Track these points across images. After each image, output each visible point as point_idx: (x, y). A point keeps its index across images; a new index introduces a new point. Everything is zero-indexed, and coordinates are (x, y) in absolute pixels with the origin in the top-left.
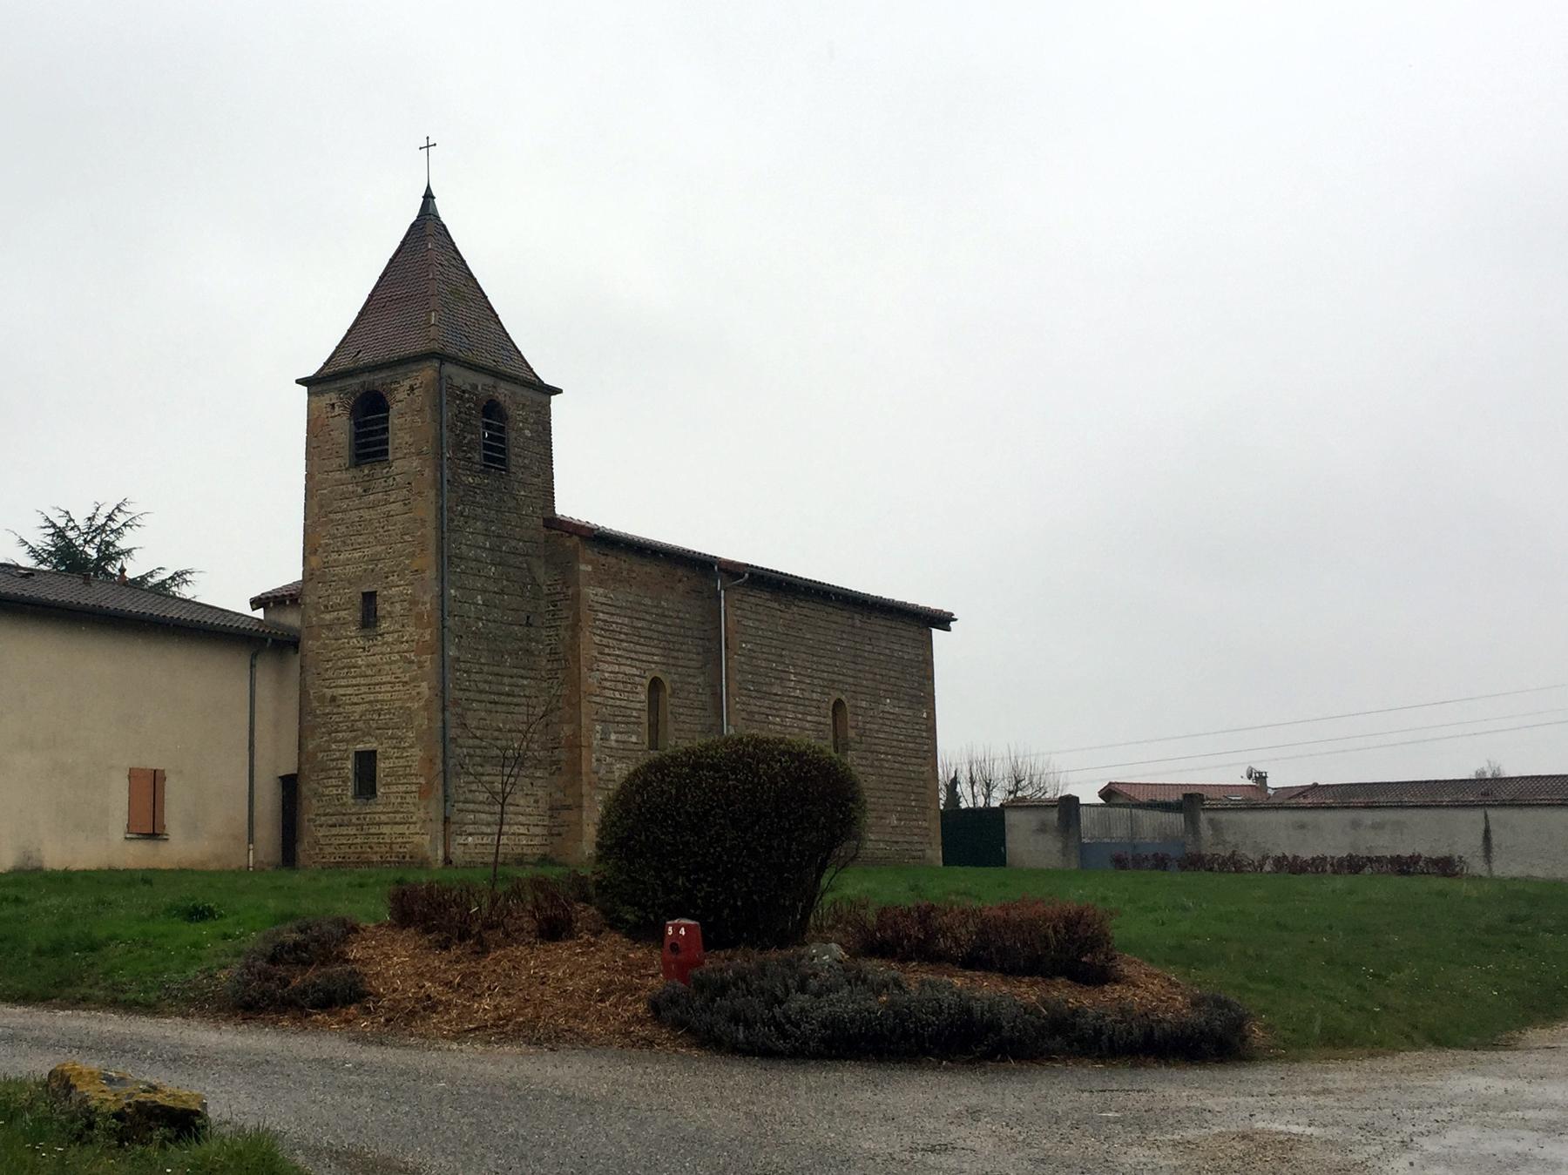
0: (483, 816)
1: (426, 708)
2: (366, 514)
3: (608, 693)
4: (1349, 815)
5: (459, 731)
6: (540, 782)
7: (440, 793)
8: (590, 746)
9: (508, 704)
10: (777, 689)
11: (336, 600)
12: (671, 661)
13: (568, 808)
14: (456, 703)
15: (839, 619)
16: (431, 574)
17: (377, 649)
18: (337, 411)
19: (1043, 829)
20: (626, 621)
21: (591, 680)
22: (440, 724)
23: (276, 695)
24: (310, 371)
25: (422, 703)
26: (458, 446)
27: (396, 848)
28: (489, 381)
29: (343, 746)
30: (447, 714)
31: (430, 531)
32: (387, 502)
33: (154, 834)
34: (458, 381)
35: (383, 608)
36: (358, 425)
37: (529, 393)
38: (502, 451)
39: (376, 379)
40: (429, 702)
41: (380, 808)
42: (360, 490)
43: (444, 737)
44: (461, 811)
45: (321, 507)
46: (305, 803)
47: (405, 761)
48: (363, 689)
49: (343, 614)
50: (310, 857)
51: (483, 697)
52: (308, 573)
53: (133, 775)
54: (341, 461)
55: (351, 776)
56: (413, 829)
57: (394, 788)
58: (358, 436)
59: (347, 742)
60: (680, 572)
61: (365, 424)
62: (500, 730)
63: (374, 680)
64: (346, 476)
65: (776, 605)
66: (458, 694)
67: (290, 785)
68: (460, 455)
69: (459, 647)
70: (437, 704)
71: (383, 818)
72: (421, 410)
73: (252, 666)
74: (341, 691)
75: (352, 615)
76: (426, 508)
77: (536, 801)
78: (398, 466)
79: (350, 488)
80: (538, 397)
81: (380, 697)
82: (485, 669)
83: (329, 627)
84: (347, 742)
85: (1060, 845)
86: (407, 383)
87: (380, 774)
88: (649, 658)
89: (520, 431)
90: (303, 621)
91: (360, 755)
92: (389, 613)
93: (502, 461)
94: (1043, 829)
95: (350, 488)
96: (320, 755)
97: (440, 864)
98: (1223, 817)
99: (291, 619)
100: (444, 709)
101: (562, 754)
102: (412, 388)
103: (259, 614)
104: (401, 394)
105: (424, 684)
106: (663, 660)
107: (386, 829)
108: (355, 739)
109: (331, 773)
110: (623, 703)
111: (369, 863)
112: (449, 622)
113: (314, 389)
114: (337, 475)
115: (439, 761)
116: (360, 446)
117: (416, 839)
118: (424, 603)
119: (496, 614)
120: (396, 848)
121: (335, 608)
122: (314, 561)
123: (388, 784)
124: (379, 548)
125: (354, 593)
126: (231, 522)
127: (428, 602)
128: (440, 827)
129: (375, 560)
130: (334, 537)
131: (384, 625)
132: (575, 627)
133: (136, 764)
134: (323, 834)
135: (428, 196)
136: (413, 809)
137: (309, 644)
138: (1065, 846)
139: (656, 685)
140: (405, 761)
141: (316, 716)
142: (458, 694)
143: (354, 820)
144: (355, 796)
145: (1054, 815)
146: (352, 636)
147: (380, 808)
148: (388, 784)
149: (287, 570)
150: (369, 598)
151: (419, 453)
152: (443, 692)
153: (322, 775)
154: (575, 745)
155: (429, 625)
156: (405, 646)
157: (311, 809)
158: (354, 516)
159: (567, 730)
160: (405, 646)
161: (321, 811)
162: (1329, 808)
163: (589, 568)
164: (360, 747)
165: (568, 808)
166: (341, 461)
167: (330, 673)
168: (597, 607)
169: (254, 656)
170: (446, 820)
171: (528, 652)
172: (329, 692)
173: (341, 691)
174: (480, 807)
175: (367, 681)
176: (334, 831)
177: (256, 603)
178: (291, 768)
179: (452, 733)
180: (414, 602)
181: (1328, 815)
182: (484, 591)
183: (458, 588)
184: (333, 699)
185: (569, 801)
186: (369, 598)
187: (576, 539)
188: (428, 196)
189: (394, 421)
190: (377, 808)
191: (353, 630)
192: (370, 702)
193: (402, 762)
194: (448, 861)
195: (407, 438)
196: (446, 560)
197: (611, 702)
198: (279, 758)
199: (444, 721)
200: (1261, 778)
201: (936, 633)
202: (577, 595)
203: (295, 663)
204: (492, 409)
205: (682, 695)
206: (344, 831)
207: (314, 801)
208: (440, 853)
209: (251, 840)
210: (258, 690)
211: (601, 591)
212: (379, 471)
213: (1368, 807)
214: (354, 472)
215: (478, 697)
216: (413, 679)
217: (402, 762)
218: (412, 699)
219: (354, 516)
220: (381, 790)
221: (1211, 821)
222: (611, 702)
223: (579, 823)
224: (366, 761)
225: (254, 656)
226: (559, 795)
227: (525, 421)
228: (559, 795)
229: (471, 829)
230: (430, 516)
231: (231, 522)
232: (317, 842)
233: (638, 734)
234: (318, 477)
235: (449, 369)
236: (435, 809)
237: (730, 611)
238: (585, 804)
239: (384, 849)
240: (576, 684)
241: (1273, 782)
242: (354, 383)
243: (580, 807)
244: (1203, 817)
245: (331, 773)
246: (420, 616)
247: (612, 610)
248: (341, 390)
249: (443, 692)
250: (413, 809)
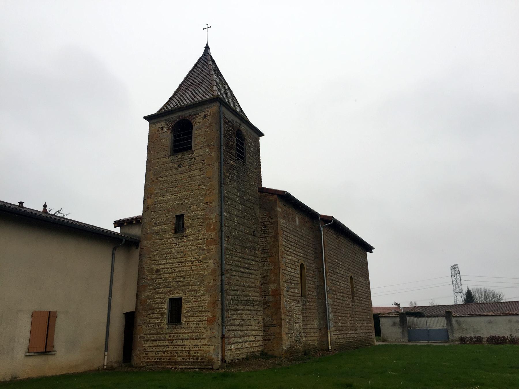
1: (212, 274)
2: (179, 177)
3: (288, 269)
4: (508, 318)
6: (259, 313)
7: (220, 322)
8: (283, 295)
9: (247, 273)
11: (161, 219)
12: (306, 256)
13: (274, 326)
14: (227, 270)
16: (215, 204)
17: (183, 244)
18: (165, 130)
19: (394, 324)
20: (292, 237)
21: (283, 262)
22: (220, 283)
23: (126, 268)
24: (154, 111)
25: (209, 271)
26: (227, 145)
27: (193, 353)
28: (239, 121)
29: (162, 296)
30: (224, 276)
31: (215, 182)
32: (191, 170)
33: (47, 350)
34: (227, 116)
35: (187, 222)
36: (175, 137)
39: (186, 114)
40: (214, 270)
41: (183, 330)
42: (176, 166)
43: (222, 290)
44: (229, 330)
45: (155, 175)
46: (139, 327)
47: (198, 304)
48: (175, 265)
49: (164, 226)
50: (140, 358)
51: (238, 269)
52: (146, 209)
53: (35, 315)
54: (166, 153)
55: (166, 312)
56: (205, 342)
57: (192, 319)
58: (175, 141)
59: (165, 293)
62: (244, 286)
63: (181, 260)
64: (168, 159)
67: (130, 319)
68: (228, 149)
69: (228, 242)
70: (218, 272)
71: (185, 336)
72: (210, 126)
73: (113, 254)
74: (162, 266)
75: (170, 227)
76: (213, 171)
77: (258, 323)
78: (196, 153)
79: (171, 165)
80: (255, 135)
81: (185, 269)
82: (238, 254)
83: (157, 233)
84: (165, 293)
85: (401, 330)
86: (202, 114)
87: (184, 311)
88: (298, 254)
89: (249, 149)
90: (142, 231)
91: (172, 301)
92: (191, 225)
94: (394, 324)
95: (171, 165)
96: (149, 301)
97: (220, 363)
98: (461, 319)
99: (135, 231)
100: (222, 275)
101: (270, 298)
102: (205, 116)
103: (118, 230)
104: (199, 119)
105: (211, 261)
107: (186, 343)
108: (169, 292)
109: (155, 311)
110: (293, 274)
111: (176, 363)
112: (224, 229)
113: (153, 121)
114: (164, 160)
115: (219, 303)
116: (175, 146)
117: (205, 348)
118: (212, 219)
119: (242, 228)
120: (193, 353)
122: (150, 201)
123: (188, 317)
124: (186, 193)
125: (172, 216)
126: (109, 187)
127: (213, 217)
128: (220, 341)
129: (183, 199)
130: (161, 189)
131: (188, 231)
132: (276, 237)
133: (37, 308)
134: (150, 348)
135: (207, 48)
136: (203, 331)
137: (145, 243)
138: (403, 331)
139: (302, 265)
140: (198, 304)
141: (148, 280)
142: (228, 267)
143: (167, 336)
144: (168, 324)
145: (398, 320)
146: (170, 237)
147: (183, 330)
148: (188, 317)
149: (136, 209)
150: (180, 218)
151: (209, 146)
152: (221, 265)
153: (150, 312)
154: (277, 293)
155: (214, 229)
156: (200, 242)
157: (142, 331)
158: (172, 178)
159: (272, 287)
160: (200, 242)
161: (148, 332)
162: (499, 315)
164: (173, 296)
165: (274, 326)
166: (166, 153)
167: (156, 257)
168: (284, 229)
169: (115, 249)
170: (223, 337)
171: (254, 248)
172: (155, 267)
173: (162, 266)
175: (178, 260)
176: (155, 343)
177: (117, 224)
178: (132, 309)
179: (226, 287)
180: (205, 219)
181: (500, 318)
182: (237, 216)
184: (158, 271)
185: (274, 322)
186: (180, 218)
187: (276, 196)
188: (207, 48)
189: (195, 132)
190: (182, 330)
191: (170, 234)
192: (179, 272)
193: (197, 304)
194: (223, 360)
195: (202, 139)
196: (221, 198)
197: (289, 273)
198: (125, 303)
199: (222, 281)
200: (398, 305)
201: (368, 254)
202: (276, 223)
203: (136, 253)
204: (239, 134)
205: (310, 271)
206: (161, 343)
207: (144, 327)
208: (220, 356)
209: (106, 350)
210: (115, 271)
211: (285, 221)
212: (187, 156)
213: (513, 315)
214: (173, 157)
216: (204, 259)
217: (197, 304)
218: (203, 269)
219: (172, 178)
220: (184, 320)
221: (457, 321)
222: (289, 273)
223: (280, 334)
224: (176, 305)
225: (115, 249)
226: (268, 319)
227: (251, 144)
228: (268, 319)
230: (216, 177)
231: (109, 187)
232: (145, 350)
233: (298, 289)
234: (153, 161)
235: (223, 109)
236: (217, 331)
237: (325, 236)
238: (283, 324)
239: (185, 354)
240: (277, 265)
241: (401, 306)
242: (174, 117)
243: (281, 326)
244: (454, 320)
245: (155, 311)
246: (209, 225)
247: (288, 231)
248: (166, 120)
249: (221, 265)
250: (203, 331)
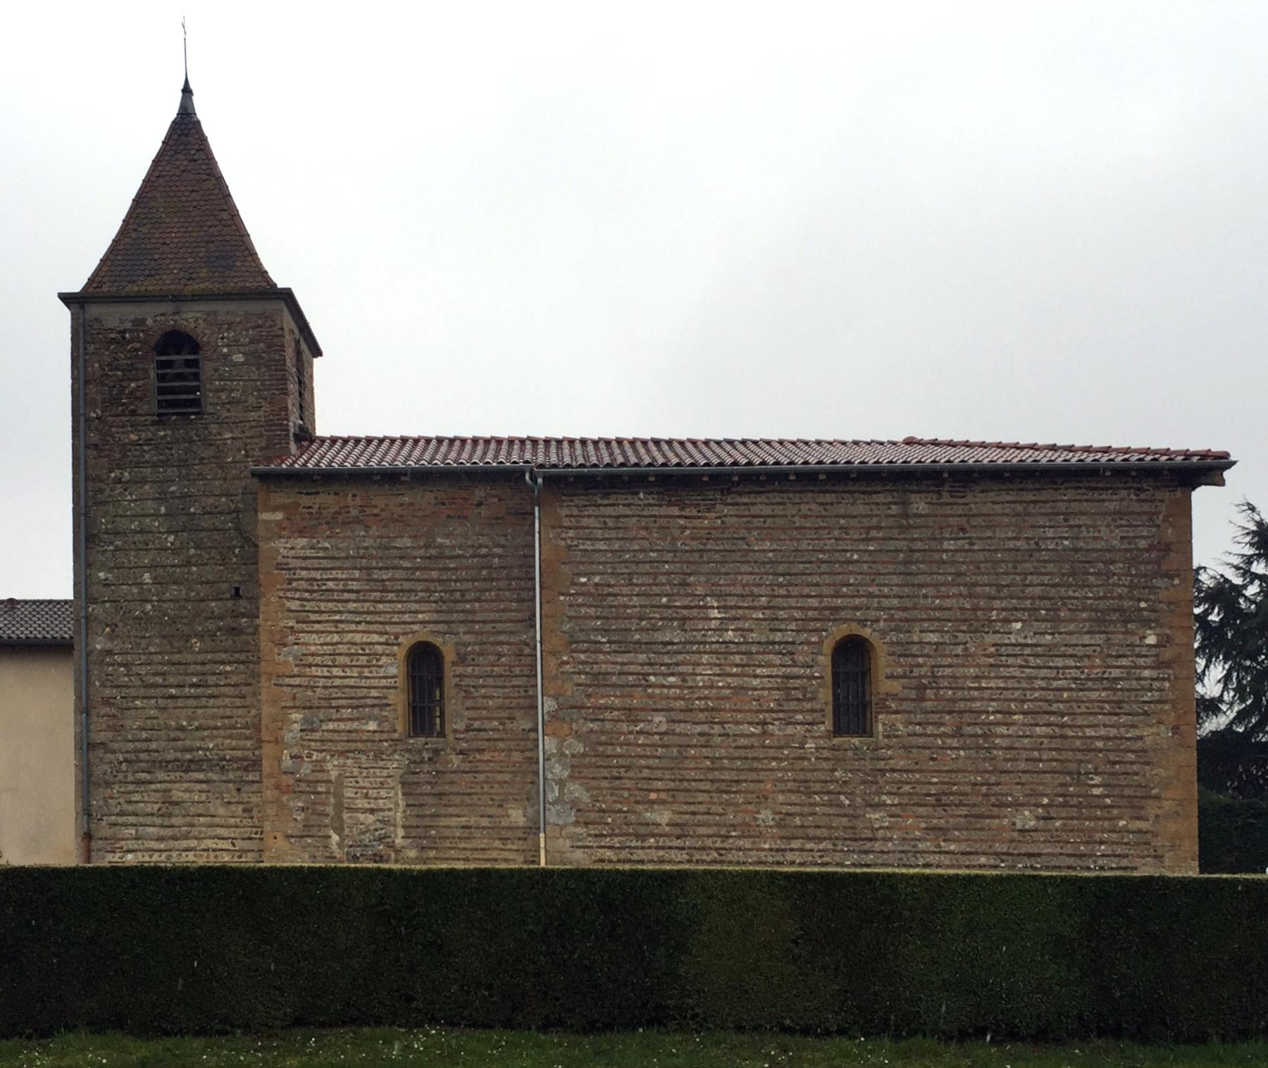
0: (150, 830)
5: (110, 735)
9: (196, 697)
10: (673, 635)
14: (107, 702)
15: (767, 510)
28: (166, 308)
34: (111, 323)
37: (254, 307)
38: (192, 390)
60: (479, 493)
61: (172, 391)
62: (182, 729)
65: (675, 511)
66: (108, 692)
93: (196, 403)
106: (435, 617)
119: (173, 591)
121: (497, 580)
163: (279, 516)
174: (149, 820)
183: (110, 570)
188: (187, 91)
211: (303, 542)
215: (142, 692)
229: (131, 844)
247: (325, 563)
